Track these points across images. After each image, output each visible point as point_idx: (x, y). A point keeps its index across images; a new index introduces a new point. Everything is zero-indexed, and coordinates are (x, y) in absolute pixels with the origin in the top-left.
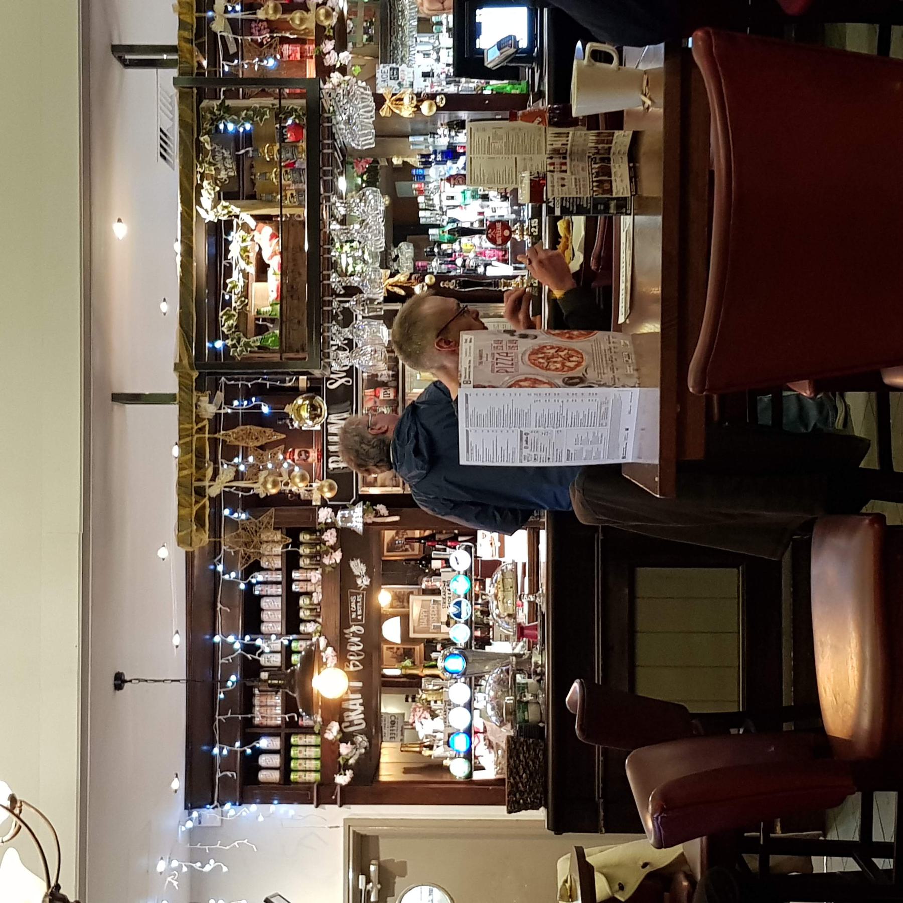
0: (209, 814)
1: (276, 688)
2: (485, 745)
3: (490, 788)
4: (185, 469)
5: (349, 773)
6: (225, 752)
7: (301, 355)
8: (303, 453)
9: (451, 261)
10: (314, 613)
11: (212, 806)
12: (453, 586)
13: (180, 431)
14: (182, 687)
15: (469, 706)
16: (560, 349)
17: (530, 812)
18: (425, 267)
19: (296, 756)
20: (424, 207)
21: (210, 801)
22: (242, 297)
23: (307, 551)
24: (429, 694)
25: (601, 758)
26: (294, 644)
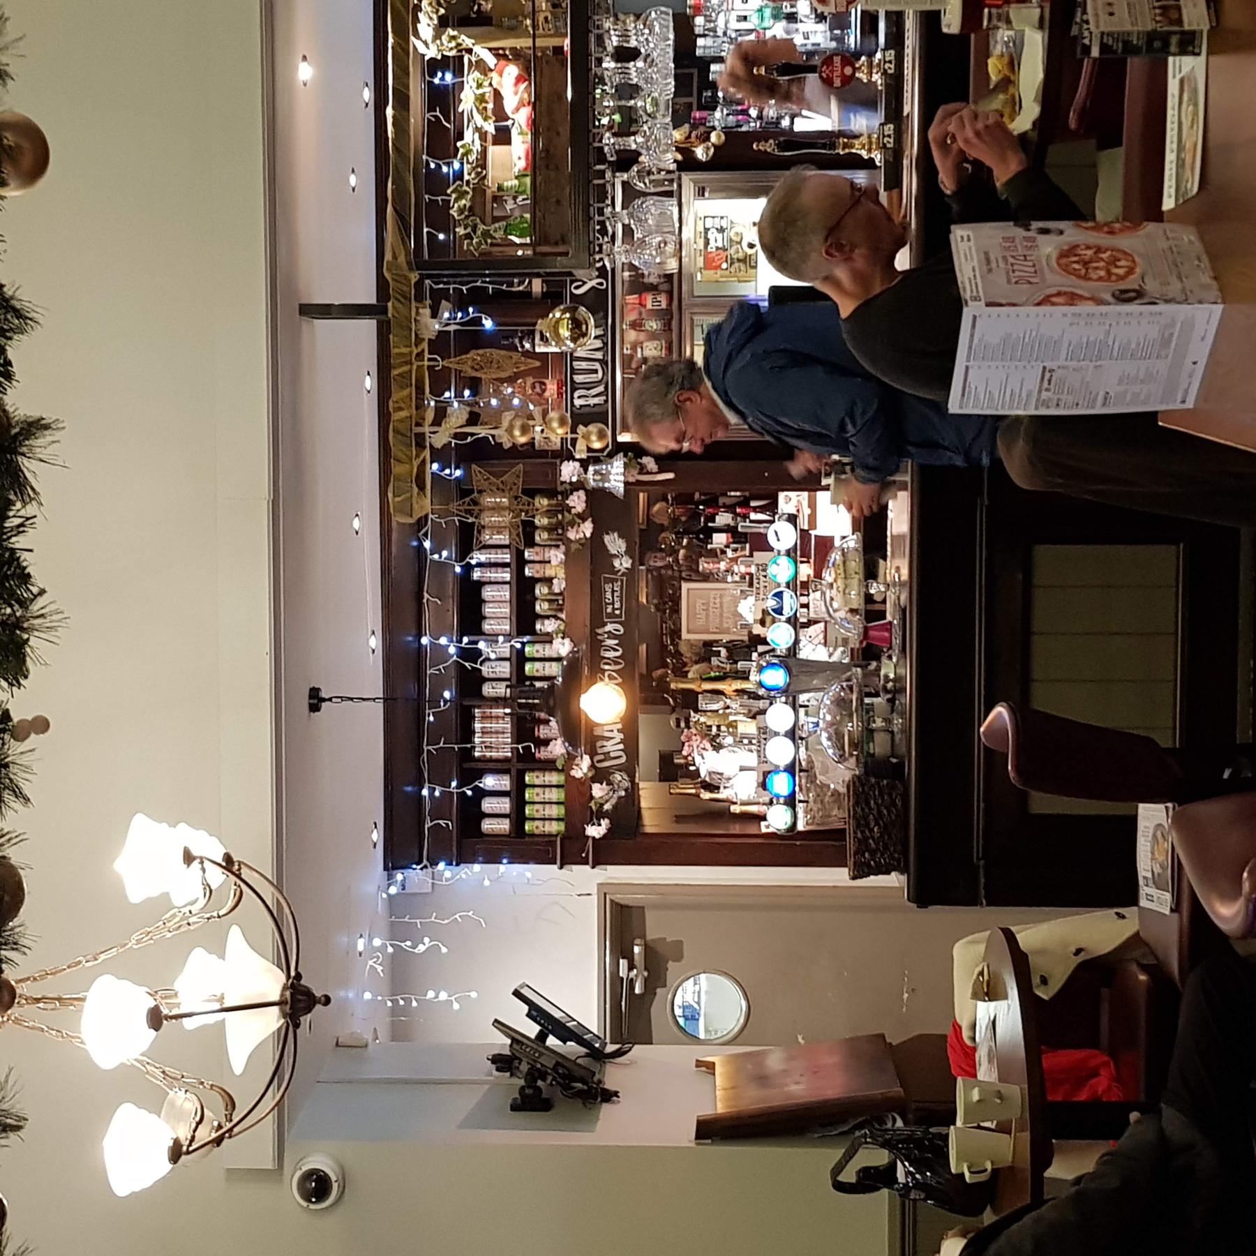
0: (416, 877)
3: (798, 843)
5: (605, 823)
6: (437, 793)
7: (561, 249)
9: (742, 110)
10: (555, 607)
11: (419, 867)
12: (772, 570)
14: (379, 706)
15: (792, 734)
16: (1099, 250)
17: (880, 877)
18: (705, 119)
20: (702, 32)
21: (417, 860)
22: (477, 166)
23: (545, 521)
25: (982, 805)
26: (527, 649)
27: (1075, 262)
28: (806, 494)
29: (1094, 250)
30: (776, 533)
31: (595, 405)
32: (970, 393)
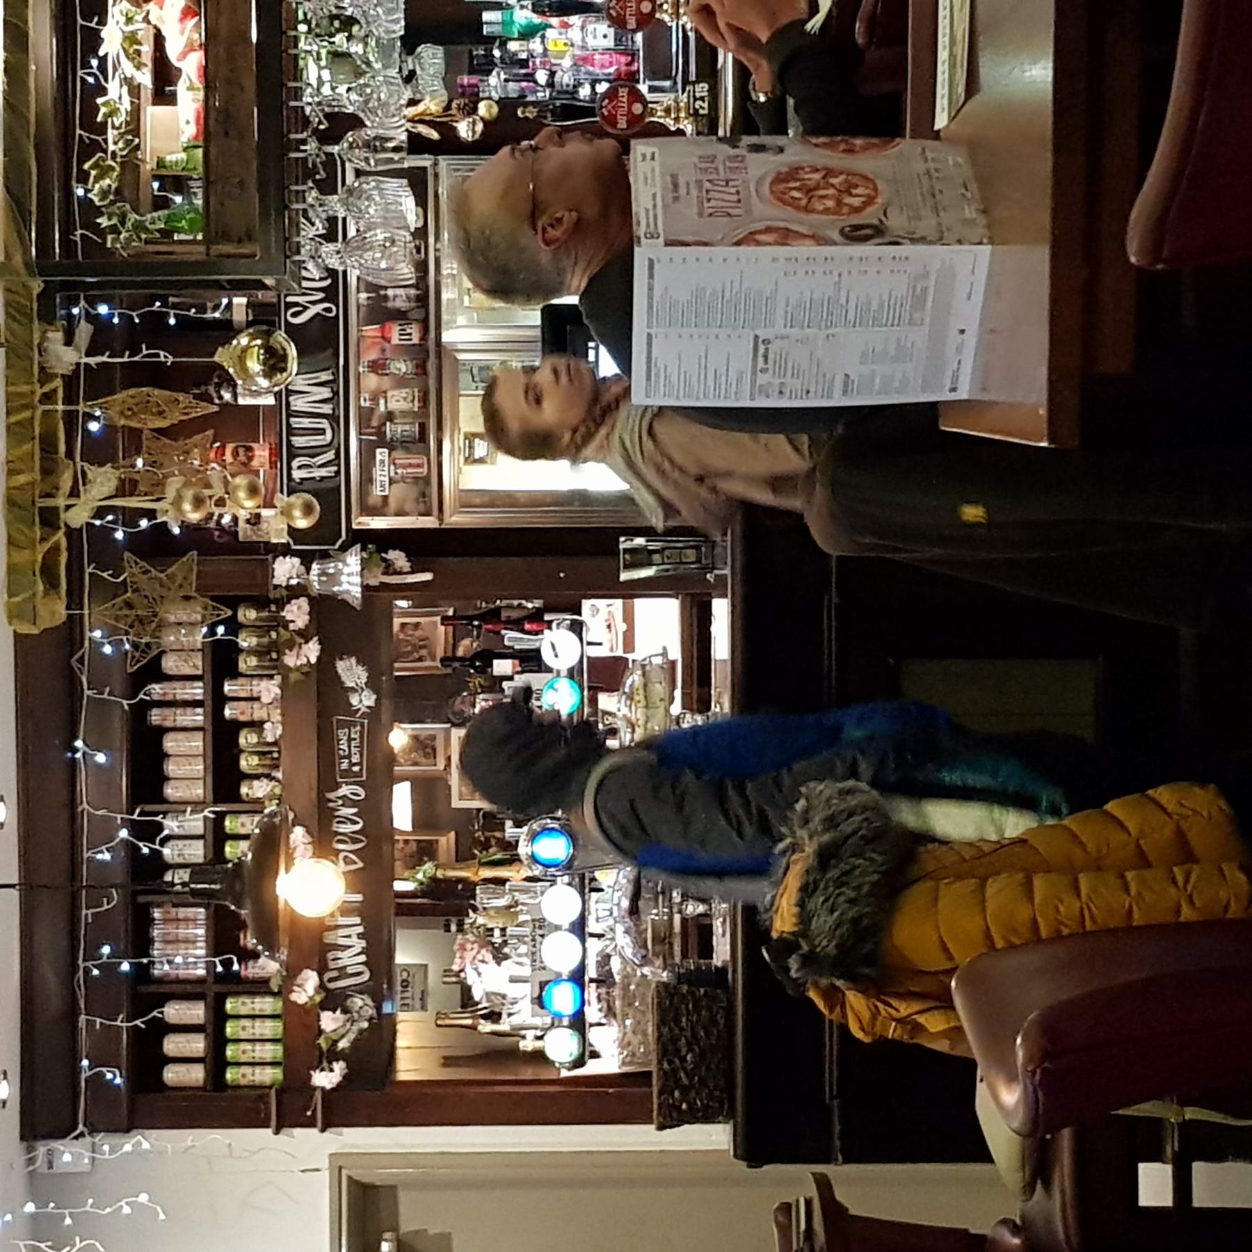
1: (198, 898)
2: (600, 1010)
3: (611, 1090)
4: (19, 472)
5: (339, 1067)
7: (246, 249)
8: (241, 451)
9: (526, 75)
10: (268, 762)
13: (9, 397)
15: (579, 928)
16: (829, 172)
18: (476, 86)
19: (234, 1037)
22: (126, 133)
23: (254, 641)
24: (491, 917)
27: (794, 189)
28: (619, 603)
29: (823, 173)
30: (553, 645)
31: (323, 478)
32: (657, 375)
